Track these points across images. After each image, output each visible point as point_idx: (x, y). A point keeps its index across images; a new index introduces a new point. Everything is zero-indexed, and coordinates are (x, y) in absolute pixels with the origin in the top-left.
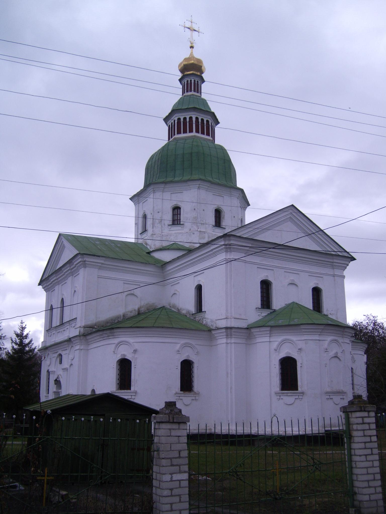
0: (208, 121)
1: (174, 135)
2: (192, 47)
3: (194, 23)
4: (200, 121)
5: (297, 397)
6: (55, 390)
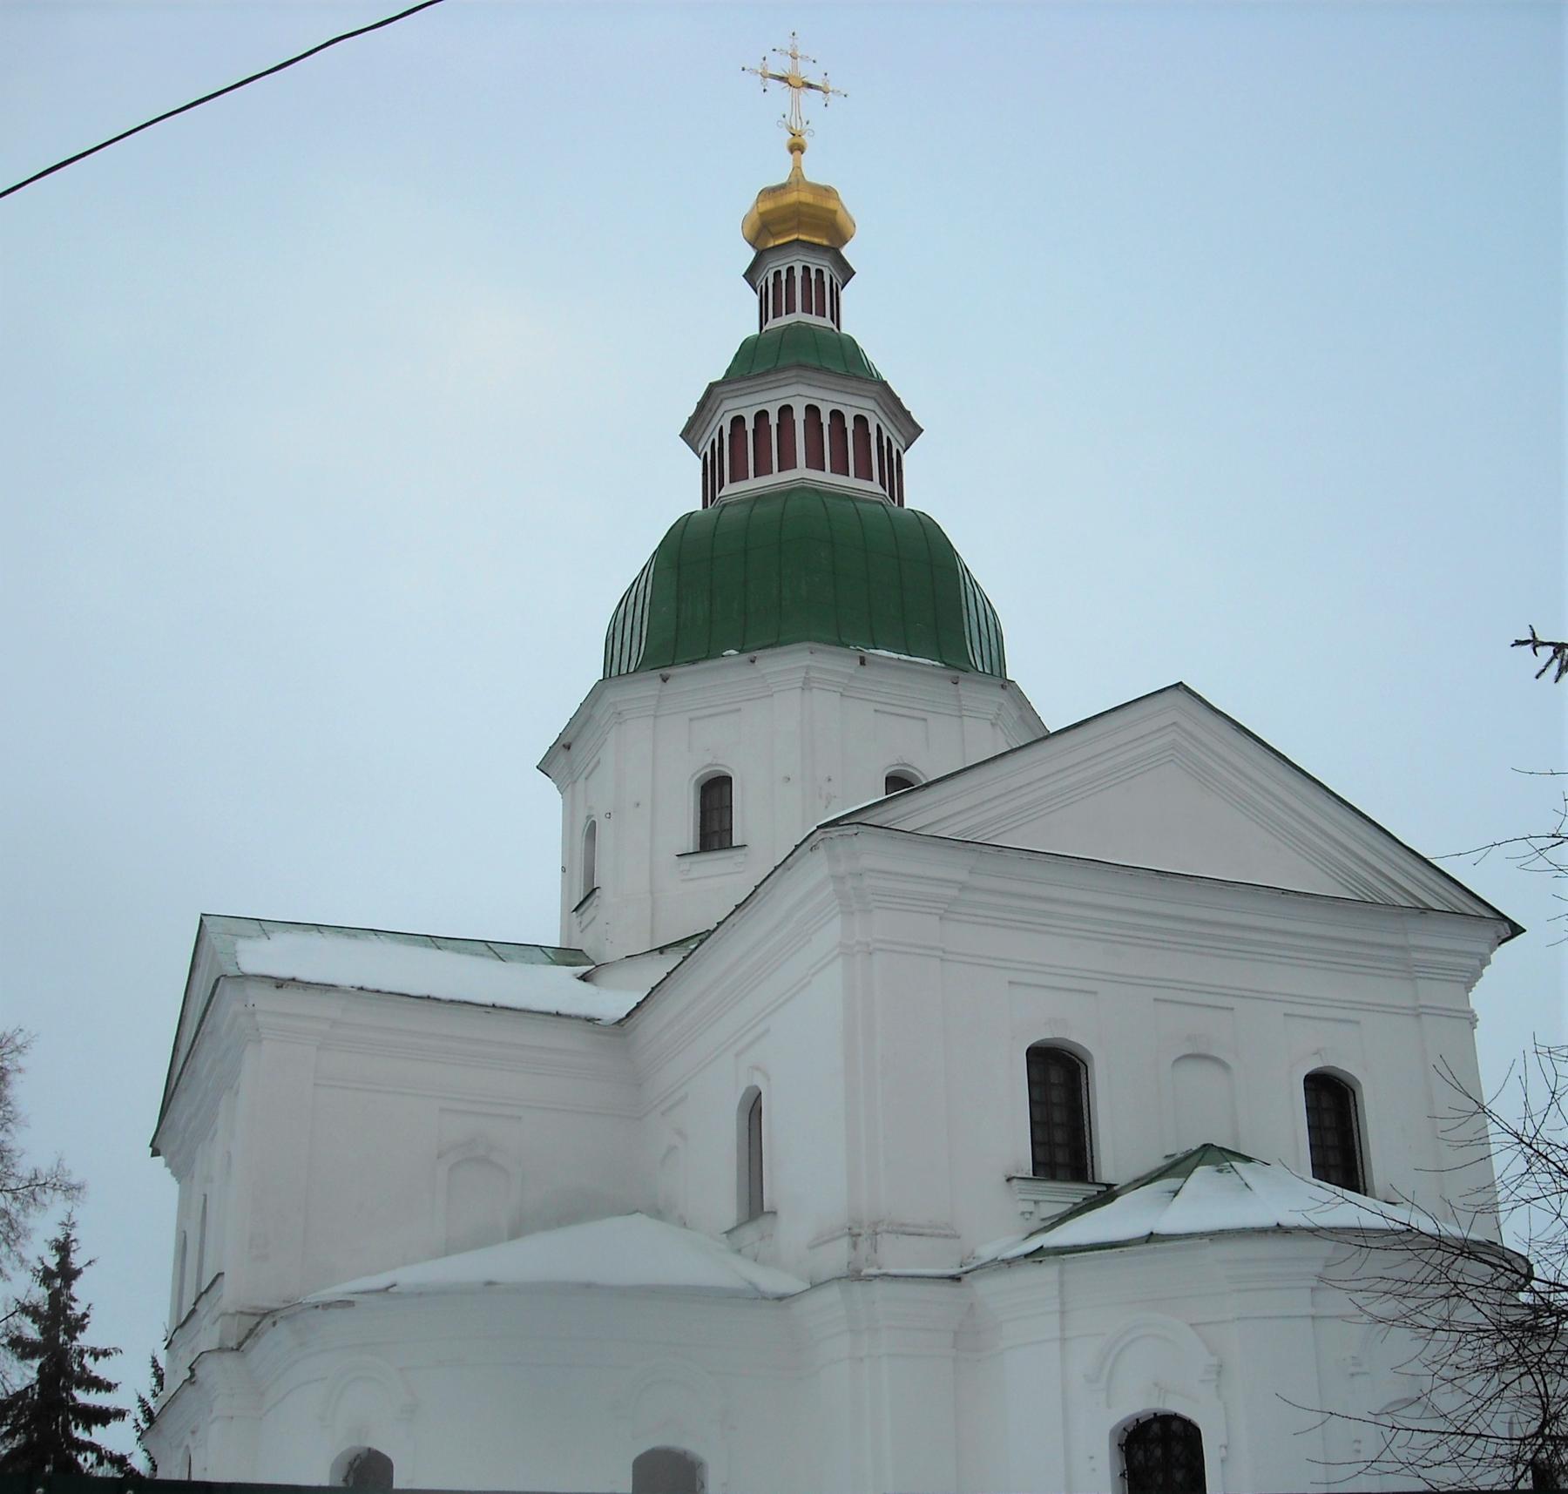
0: (860, 421)
1: (722, 485)
2: (797, 148)
4: (826, 420)
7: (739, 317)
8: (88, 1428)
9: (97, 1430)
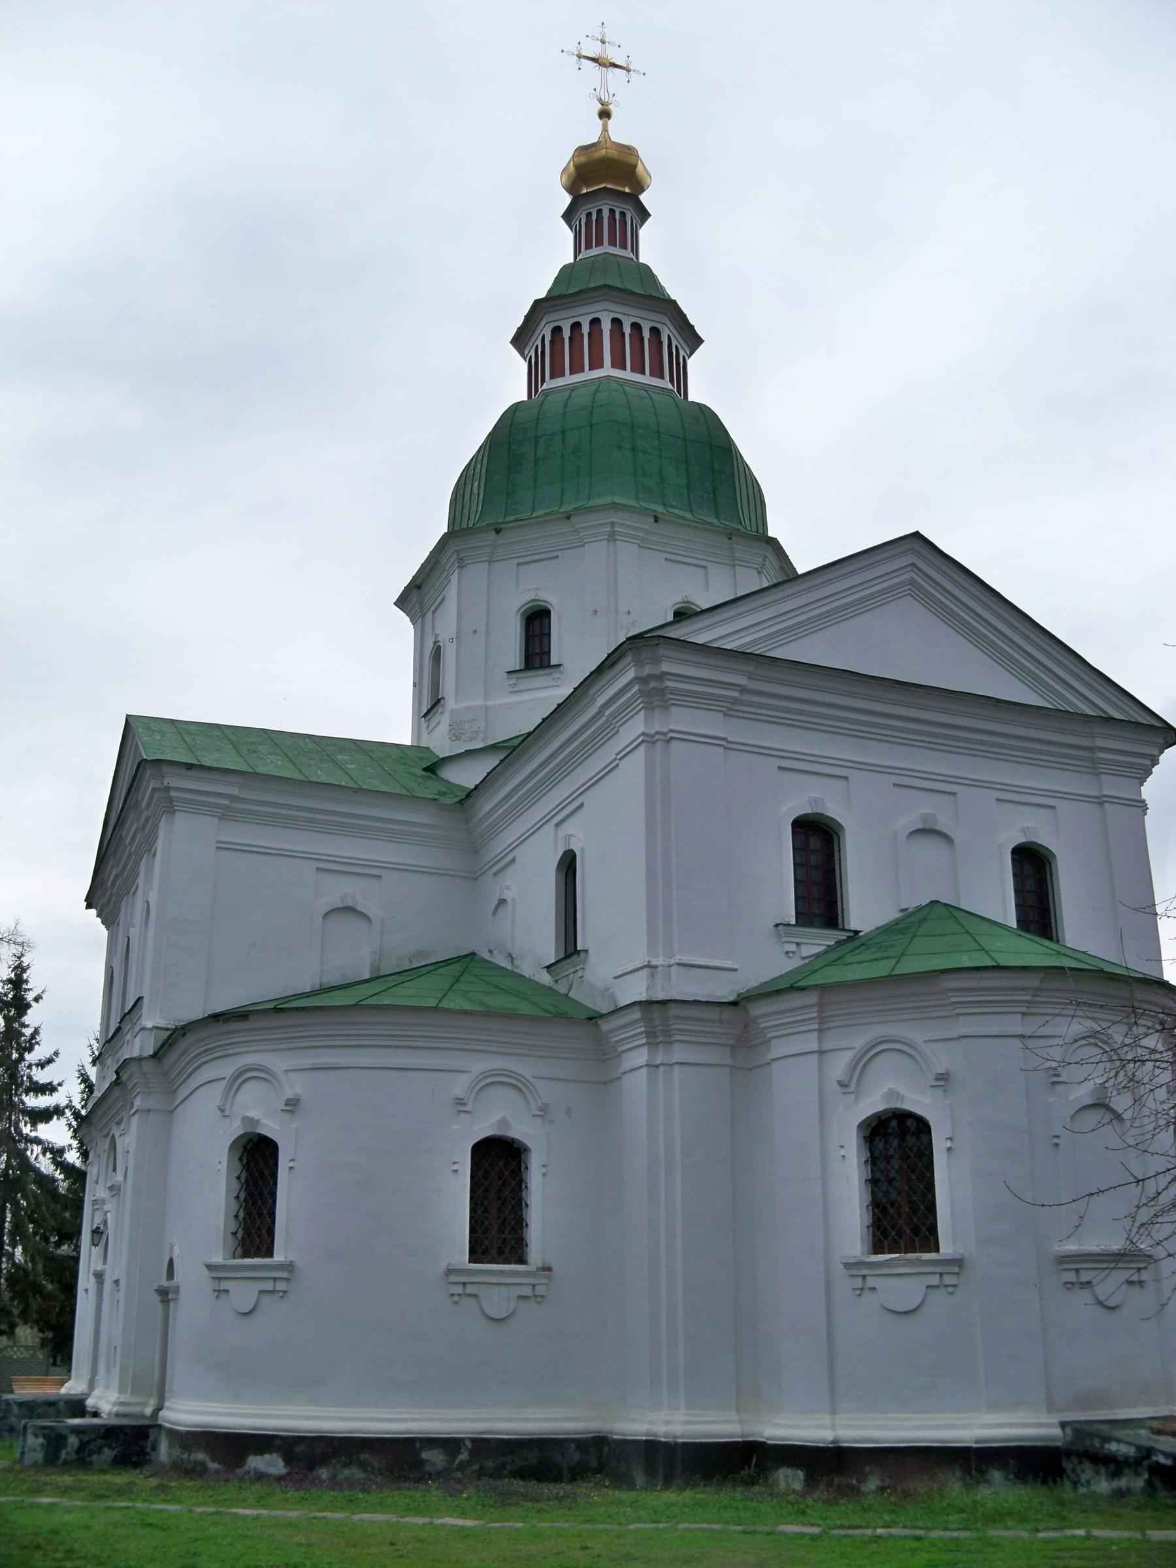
1: (543, 381)
2: (605, 114)
3: (612, 43)
5: (935, 1280)
6: (218, 1259)
7: (559, 248)
8: (34, 1125)
9: (41, 1127)
